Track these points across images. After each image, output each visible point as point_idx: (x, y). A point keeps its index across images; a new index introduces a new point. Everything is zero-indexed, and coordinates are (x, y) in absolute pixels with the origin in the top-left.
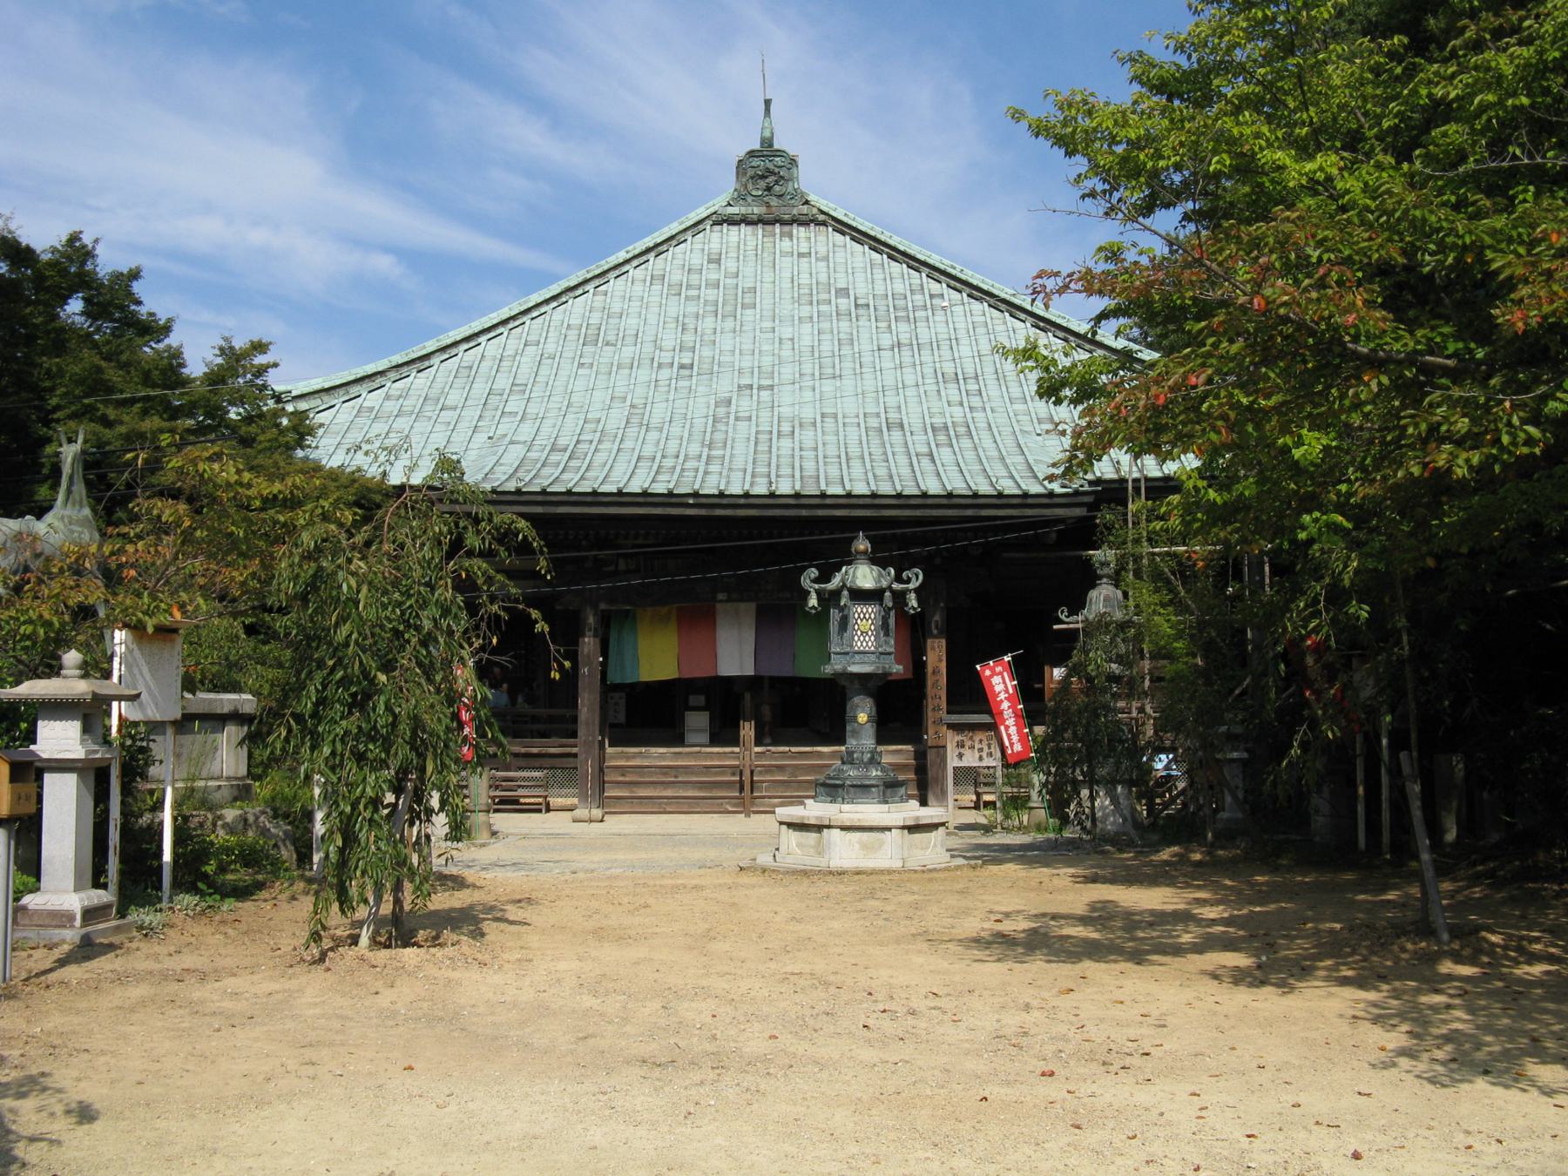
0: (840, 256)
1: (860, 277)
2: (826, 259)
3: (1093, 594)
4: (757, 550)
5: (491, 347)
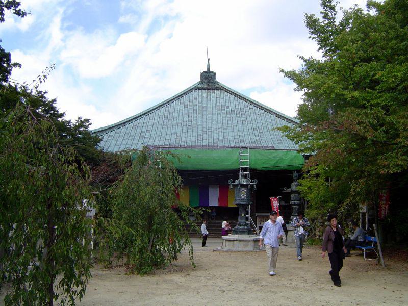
2: (223, 99)
3: (293, 184)
5: (141, 121)
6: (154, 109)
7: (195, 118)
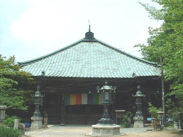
0: (100, 46)
1: (102, 49)
3: (137, 92)
4: (91, 85)
6: (59, 52)
7: (81, 56)
